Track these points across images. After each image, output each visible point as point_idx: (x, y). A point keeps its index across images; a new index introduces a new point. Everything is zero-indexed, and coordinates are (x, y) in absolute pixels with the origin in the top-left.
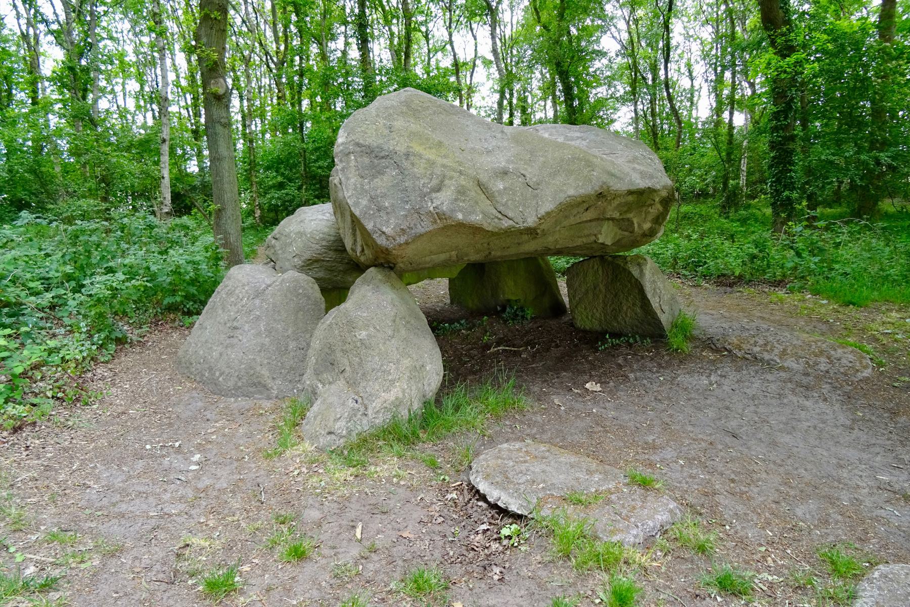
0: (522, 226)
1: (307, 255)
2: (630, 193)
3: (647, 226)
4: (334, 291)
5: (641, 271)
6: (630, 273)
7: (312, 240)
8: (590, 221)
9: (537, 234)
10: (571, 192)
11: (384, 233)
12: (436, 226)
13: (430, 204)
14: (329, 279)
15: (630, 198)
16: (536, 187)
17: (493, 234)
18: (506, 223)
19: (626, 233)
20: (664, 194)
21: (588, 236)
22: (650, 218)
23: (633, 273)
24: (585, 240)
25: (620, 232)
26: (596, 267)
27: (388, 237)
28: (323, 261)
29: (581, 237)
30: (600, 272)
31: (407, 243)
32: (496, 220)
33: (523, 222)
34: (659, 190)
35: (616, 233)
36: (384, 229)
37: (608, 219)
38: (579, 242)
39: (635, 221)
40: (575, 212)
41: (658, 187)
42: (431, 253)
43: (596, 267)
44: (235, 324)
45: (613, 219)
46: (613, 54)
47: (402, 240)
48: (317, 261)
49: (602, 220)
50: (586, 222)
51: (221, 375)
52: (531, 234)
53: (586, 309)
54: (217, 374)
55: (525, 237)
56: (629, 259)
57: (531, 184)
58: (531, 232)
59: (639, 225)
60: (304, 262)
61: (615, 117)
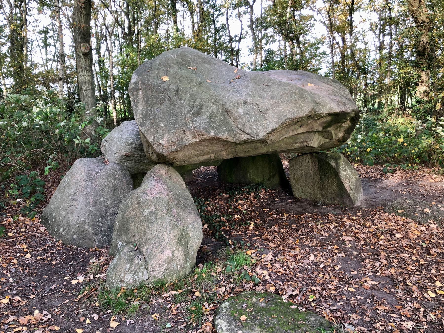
0: (255, 139)
1: (123, 152)
2: (330, 114)
3: (341, 135)
4: (136, 178)
5: (337, 164)
6: (330, 164)
7: (126, 144)
8: (303, 133)
9: (267, 143)
10: (290, 116)
11: (160, 144)
12: (195, 140)
13: (191, 125)
14: (137, 168)
15: (329, 118)
16: (266, 112)
17: (236, 144)
18: (245, 137)
19: (328, 140)
20: (353, 115)
21: (302, 142)
22: (343, 130)
23: (332, 164)
24: (299, 145)
25: (322, 139)
26: (307, 160)
27: (163, 147)
28: (134, 156)
29: (297, 143)
30: (310, 163)
31: (176, 151)
32: (238, 135)
33: (257, 136)
34: (349, 113)
35: (320, 140)
36: (161, 141)
37: (315, 132)
38: (296, 146)
39: (333, 132)
40: (292, 128)
41: (349, 110)
42: (196, 156)
43: (307, 160)
44: (75, 197)
45: (318, 132)
46: (379, 22)
47: (174, 148)
48: (129, 156)
49: (311, 132)
50: (301, 133)
51: (64, 230)
52: (263, 143)
53: (301, 186)
54: (61, 230)
55: (259, 145)
56: (329, 155)
57: (263, 110)
58: (263, 141)
59: (336, 135)
60: (121, 157)
61: (320, 66)
